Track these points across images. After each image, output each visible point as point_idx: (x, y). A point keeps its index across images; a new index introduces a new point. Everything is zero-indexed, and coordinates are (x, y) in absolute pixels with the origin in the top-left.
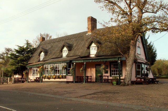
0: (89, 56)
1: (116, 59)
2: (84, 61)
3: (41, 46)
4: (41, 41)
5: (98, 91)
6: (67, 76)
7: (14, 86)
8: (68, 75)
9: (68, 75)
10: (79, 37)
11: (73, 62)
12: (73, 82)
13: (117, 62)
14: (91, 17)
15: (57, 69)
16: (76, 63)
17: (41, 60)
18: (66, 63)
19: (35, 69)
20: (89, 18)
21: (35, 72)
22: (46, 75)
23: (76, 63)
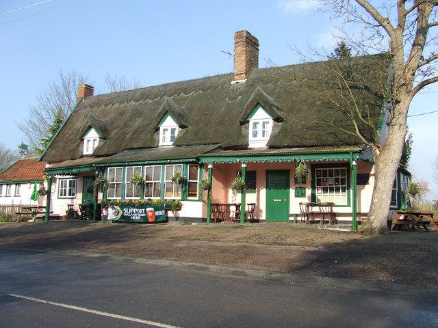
0: (242, 147)
1: (346, 158)
2: (243, 159)
3: (83, 112)
4: (82, 95)
5: (139, 225)
6: (182, 202)
7: (40, 253)
8: (187, 200)
9: (189, 198)
10: (210, 88)
11: (203, 160)
12: (204, 220)
13: (347, 164)
14: (248, 33)
15: (153, 181)
16: (216, 166)
17: (87, 151)
18: (183, 163)
19: (68, 181)
20: (239, 35)
21: (68, 188)
22: (152, 198)
23: (216, 166)
